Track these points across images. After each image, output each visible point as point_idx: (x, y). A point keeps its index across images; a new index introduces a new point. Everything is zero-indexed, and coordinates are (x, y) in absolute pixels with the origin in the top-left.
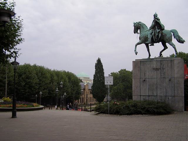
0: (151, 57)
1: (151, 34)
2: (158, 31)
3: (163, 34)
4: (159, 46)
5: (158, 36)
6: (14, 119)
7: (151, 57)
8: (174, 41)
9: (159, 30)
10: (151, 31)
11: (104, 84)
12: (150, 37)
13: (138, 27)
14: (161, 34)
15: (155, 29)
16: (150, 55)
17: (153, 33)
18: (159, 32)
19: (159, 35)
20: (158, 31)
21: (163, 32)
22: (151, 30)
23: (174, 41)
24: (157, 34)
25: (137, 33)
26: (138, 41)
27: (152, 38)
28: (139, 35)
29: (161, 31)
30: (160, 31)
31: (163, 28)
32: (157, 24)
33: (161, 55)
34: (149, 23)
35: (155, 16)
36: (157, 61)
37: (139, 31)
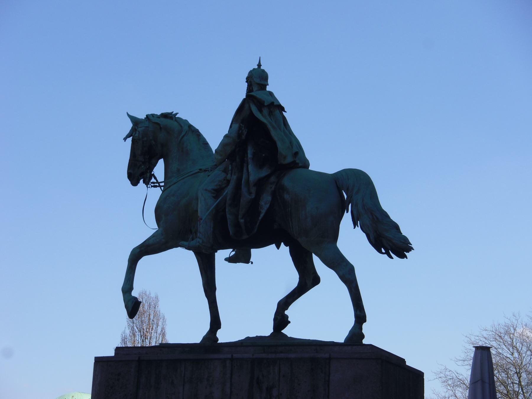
0: (288, 331)
1: (217, 192)
2: (253, 173)
3: (286, 197)
4: (274, 264)
5: (255, 204)
6: (240, 266)
7: (224, 336)
8: (351, 240)
9: (264, 172)
10: (218, 175)
11: (299, 160)
12: (204, 207)
13: (155, 142)
14: (274, 195)
15: (241, 166)
16: (216, 323)
17: (229, 190)
18: (260, 184)
19: (262, 203)
20: (253, 173)
21: (286, 181)
22: (222, 167)
23: (351, 240)
24: (246, 197)
25: (146, 183)
26: (148, 228)
27: (219, 216)
28: (155, 194)
29: (273, 179)
30: (268, 177)
31: (289, 159)
32: (260, 117)
33: (281, 321)
34: (215, 127)
35: (257, 80)
36: (232, 359)
37: (159, 170)
